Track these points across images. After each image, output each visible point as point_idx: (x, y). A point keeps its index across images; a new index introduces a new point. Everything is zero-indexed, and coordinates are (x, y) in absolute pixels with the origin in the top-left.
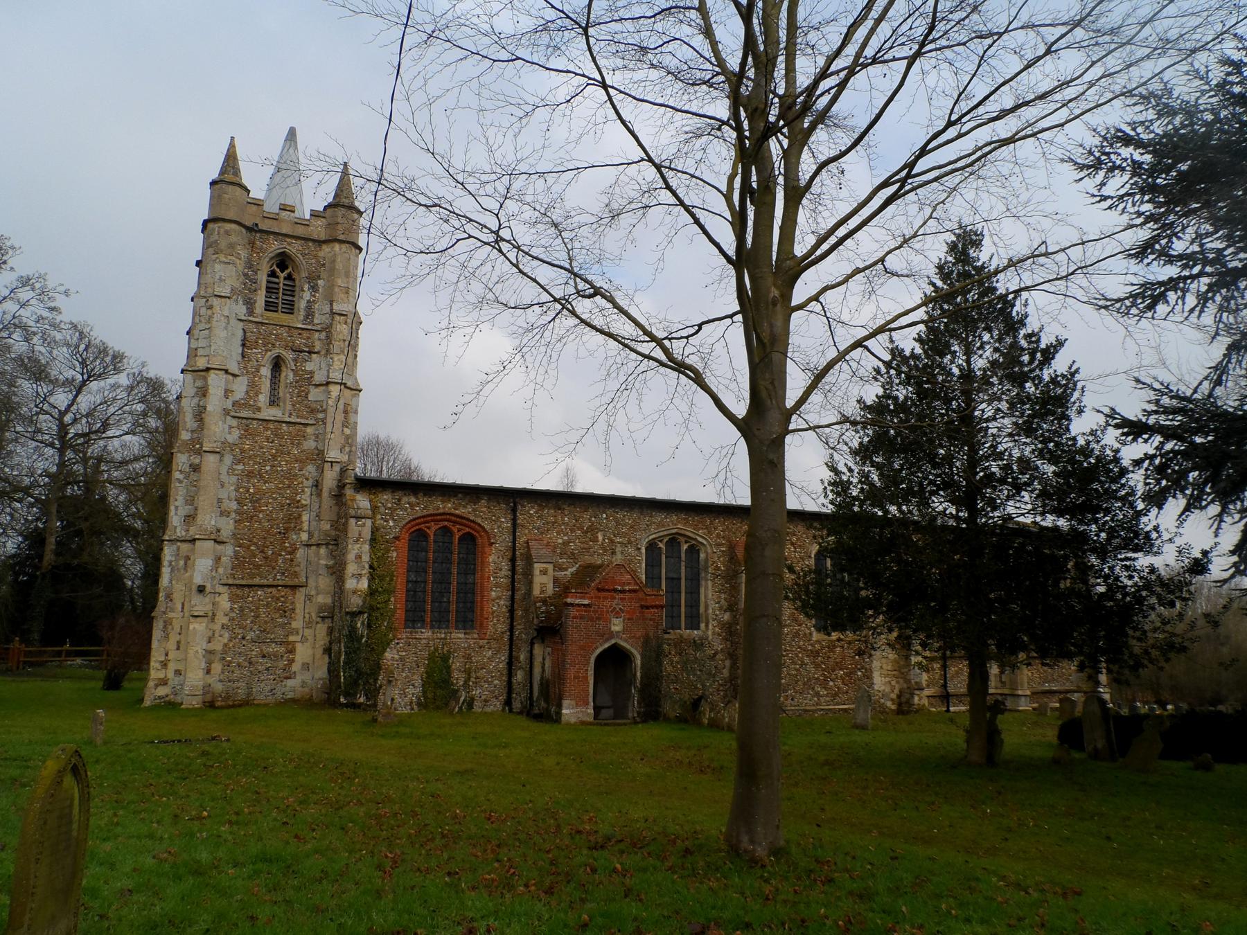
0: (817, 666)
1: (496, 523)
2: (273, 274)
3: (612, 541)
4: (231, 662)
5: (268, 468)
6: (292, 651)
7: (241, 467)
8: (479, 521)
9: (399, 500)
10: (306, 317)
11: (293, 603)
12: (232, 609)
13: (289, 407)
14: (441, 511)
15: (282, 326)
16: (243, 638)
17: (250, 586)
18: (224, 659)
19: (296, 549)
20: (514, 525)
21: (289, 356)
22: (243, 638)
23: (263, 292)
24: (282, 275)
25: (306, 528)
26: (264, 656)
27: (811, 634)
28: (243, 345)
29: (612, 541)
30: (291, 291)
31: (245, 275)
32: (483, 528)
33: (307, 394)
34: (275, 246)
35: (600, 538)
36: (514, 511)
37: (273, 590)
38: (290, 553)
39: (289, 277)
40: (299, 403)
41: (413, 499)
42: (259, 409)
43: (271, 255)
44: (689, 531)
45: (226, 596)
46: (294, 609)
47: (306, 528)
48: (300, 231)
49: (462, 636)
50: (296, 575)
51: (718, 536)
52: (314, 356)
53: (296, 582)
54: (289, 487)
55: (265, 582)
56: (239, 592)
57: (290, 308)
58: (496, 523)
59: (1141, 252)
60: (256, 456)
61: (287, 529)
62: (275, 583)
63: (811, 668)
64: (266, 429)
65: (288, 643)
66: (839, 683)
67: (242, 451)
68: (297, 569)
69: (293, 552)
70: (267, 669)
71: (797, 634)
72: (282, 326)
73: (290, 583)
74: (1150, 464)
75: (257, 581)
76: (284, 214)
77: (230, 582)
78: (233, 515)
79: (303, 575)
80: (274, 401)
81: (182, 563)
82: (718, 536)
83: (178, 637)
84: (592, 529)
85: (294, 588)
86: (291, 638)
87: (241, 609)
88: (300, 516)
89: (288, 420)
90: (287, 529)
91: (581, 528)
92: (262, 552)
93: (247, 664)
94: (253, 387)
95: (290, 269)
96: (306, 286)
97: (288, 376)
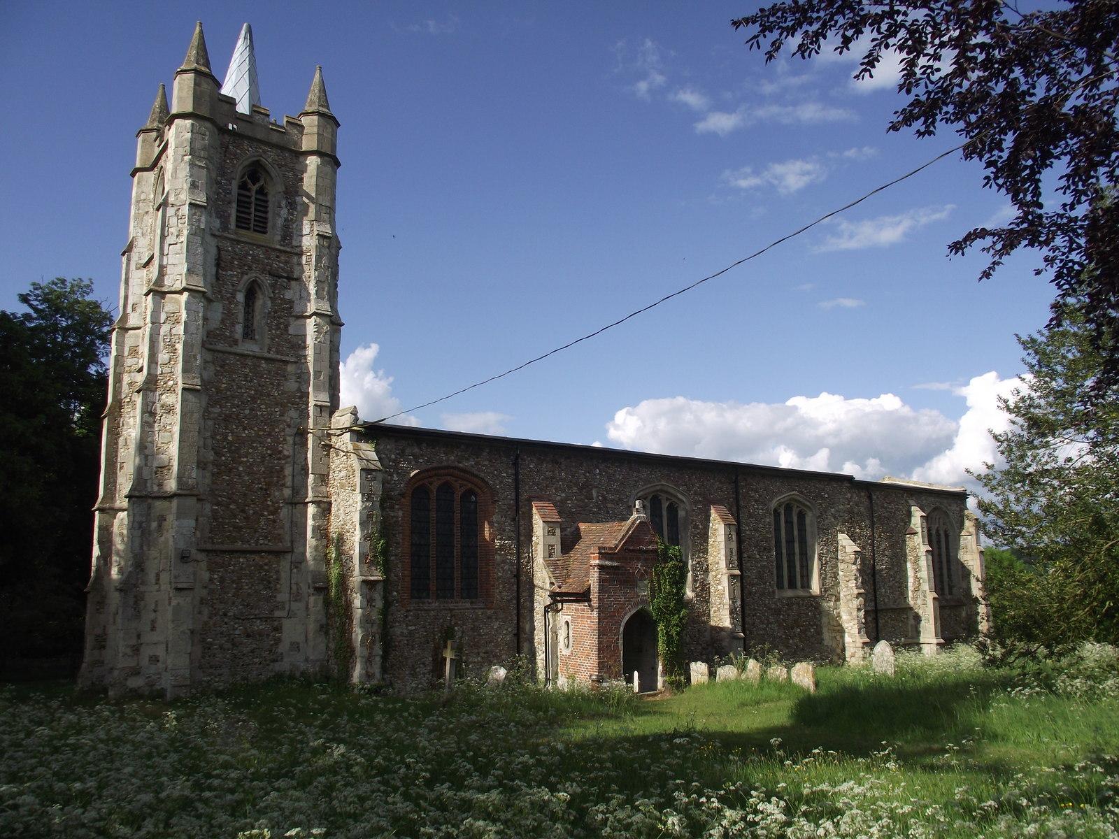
0: (780, 625)
1: (499, 476)
2: (243, 186)
3: (605, 498)
4: (211, 644)
5: (247, 412)
6: (278, 629)
7: (217, 410)
8: (482, 475)
9: (403, 451)
10: (284, 238)
11: (277, 572)
12: (211, 580)
13: (267, 341)
14: (445, 464)
15: (259, 246)
16: (225, 615)
17: (232, 552)
18: (204, 640)
19: (280, 508)
20: (517, 481)
21: (267, 280)
22: (225, 615)
23: (234, 205)
24: (254, 188)
25: (289, 483)
26: (248, 636)
27: (774, 592)
28: (218, 265)
29: (605, 498)
30: (263, 206)
31: (218, 183)
32: (487, 483)
33: (287, 326)
34: (250, 153)
35: (595, 495)
36: (515, 464)
37: (257, 557)
38: (272, 513)
39: (261, 191)
40: (278, 336)
41: (416, 450)
42: (236, 342)
43: (246, 163)
44: (670, 486)
45: (204, 565)
46: (278, 579)
47: (289, 483)
48: (275, 138)
49: (468, 605)
50: (279, 538)
51: (696, 493)
52: (293, 283)
53: (280, 546)
54: (269, 435)
55: (246, 547)
56: (218, 559)
57: (262, 226)
58: (499, 476)
59: (1005, 140)
60: (233, 397)
61: (269, 484)
62: (259, 548)
63: (775, 626)
64: (245, 366)
65: (273, 619)
66: (797, 640)
67: (218, 391)
68: (280, 531)
69: (275, 512)
70: (253, 651)
71: (763, 594)
72: (259, 246)
73: (275, 548)
74: (1075, 388)
75: (239, 545)
76: (258, 117)
77: (209, 546)
78: (210, 467)
79: (288, 538)
80: (248, 334)
81: (154, 525)
82: (696, 493)
83: (152, 616)
84: (586, 487)
85: (279, 553)
86: (277, 614)
87: (222, 580)
88: (282, 469)
89: (266, 355)
90: (269, 484)
91: (576, 485)
92: (243, 511)
93: (229, 645)
94: (228, 315)
95: (262, 182)
96: (284, 203)
97: (263, 303)
